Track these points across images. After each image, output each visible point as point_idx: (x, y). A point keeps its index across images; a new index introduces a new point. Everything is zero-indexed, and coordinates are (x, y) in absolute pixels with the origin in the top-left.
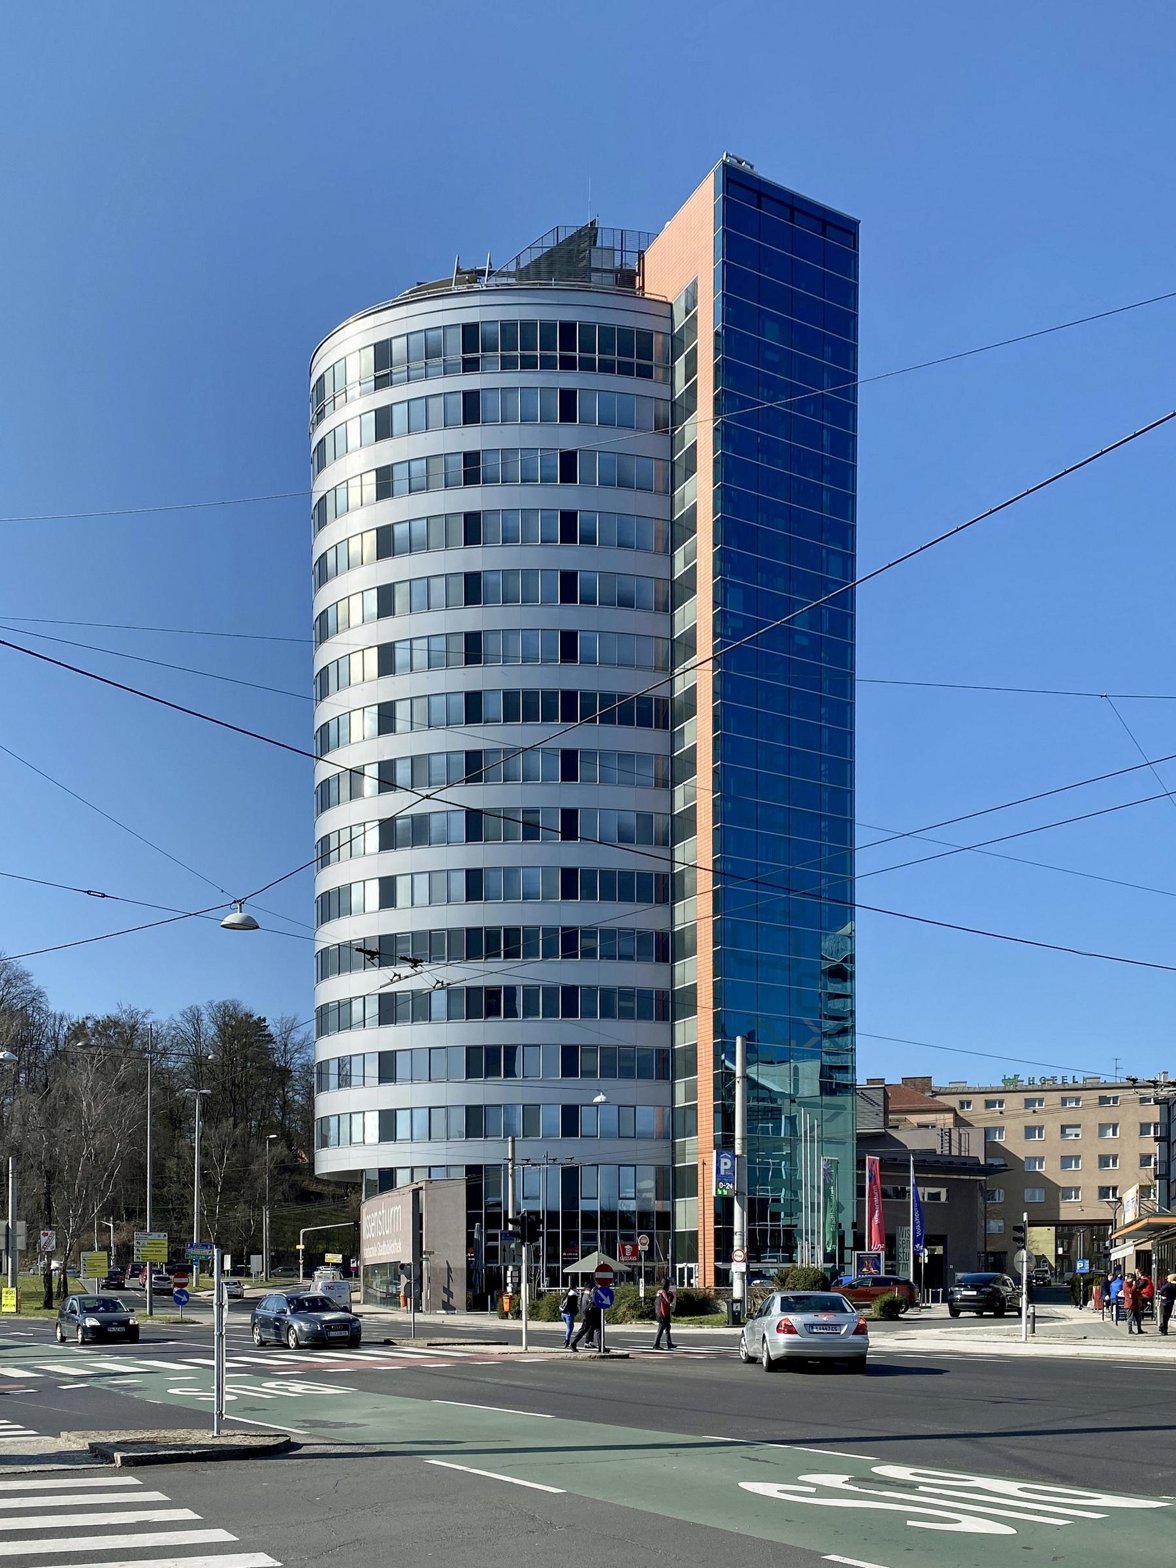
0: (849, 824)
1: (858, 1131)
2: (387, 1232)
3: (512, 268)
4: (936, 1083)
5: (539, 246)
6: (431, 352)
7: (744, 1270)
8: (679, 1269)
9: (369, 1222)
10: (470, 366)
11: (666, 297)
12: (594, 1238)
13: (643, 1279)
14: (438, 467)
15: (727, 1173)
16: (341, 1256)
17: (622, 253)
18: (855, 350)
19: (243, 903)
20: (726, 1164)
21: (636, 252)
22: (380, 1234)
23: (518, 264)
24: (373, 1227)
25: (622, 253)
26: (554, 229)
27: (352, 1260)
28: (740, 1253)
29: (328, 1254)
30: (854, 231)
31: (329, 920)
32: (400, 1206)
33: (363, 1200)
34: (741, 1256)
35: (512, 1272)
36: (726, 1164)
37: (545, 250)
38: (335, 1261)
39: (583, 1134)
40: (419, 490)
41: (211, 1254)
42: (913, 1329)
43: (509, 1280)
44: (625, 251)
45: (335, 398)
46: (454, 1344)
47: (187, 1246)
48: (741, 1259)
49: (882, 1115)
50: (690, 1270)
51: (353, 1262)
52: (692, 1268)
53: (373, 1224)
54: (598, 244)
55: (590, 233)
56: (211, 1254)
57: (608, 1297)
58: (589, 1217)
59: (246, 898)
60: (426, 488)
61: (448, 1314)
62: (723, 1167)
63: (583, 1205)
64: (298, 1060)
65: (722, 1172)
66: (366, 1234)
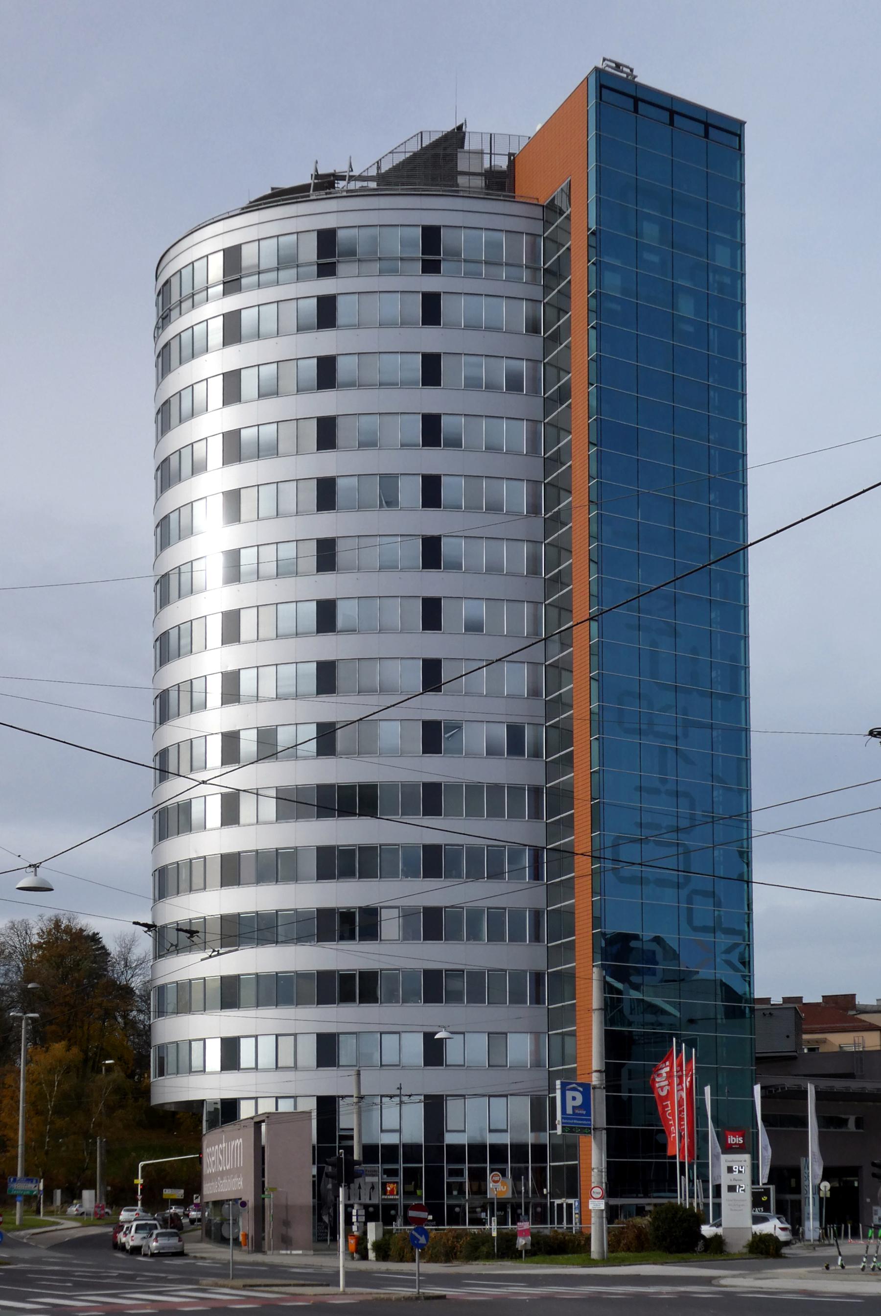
0: (744, 733)
1: (757, 1055)
2: (228, 1167)
3: (373, 172)
4: (860, 1001)
5: (401, 151)
6: (285, 262)
7: (603, 1207)
8: (557, 1204)
9: (211, 1155)
10: (326, 270)
11: (538, 199)
12: (460, 1173)
13: (496, 1218)
14: (290, 370)
15: (577, 1111)
16: (182, 1191)
17: (491, 156)
18: (742, 249)
19: (38, 867)
20: (574, 1098)
21: (506, 155)
22: (221, 1169)
23: (379, 168)
24: (214, 1161)
25: (491, 156)
26: (418, 134)
27: (195, 1196)
28: (598, 1190)
29: (167, 1190)
30: (739, 133)
31: (168, 837)
32: (241, 1139)
33: (204, 1132)
34: (599, 1193)
35: (357, 1211)
36: (574, 1098)
37: (408, 155)
38: (176, 1197)
39: (448, 1064)
40: (271, 395)
41: (37, 1188)
42: (782, 1267)
43: (354, 1219)
44: (494, 154)
45: (181, 302)
46: (289, 1285)
47: (10, 1181)
48: (599, 1196)
49: (792, 1037)
50: (570, 1206)
51: (197, 1198)
52: (572, 1204)
53: (213, 1159)
54: (466, 147)
55: (457, 136)
56: (37, 1188)
57: (423, 1236)
58: (456, 1152)
59: (41, 863)
60: (276, 393)
61: (306, 1255)
62: (570, 1104)
63: (450, 1139)
64: (136, 983)
65: (569, 1111)
66: (208, 1169)
